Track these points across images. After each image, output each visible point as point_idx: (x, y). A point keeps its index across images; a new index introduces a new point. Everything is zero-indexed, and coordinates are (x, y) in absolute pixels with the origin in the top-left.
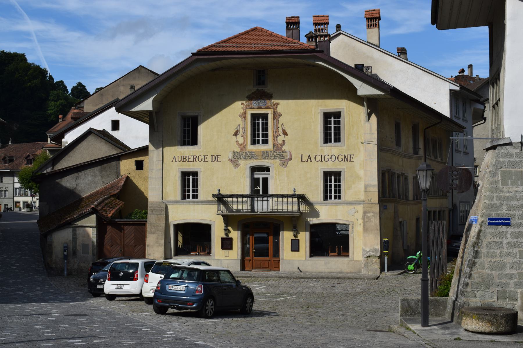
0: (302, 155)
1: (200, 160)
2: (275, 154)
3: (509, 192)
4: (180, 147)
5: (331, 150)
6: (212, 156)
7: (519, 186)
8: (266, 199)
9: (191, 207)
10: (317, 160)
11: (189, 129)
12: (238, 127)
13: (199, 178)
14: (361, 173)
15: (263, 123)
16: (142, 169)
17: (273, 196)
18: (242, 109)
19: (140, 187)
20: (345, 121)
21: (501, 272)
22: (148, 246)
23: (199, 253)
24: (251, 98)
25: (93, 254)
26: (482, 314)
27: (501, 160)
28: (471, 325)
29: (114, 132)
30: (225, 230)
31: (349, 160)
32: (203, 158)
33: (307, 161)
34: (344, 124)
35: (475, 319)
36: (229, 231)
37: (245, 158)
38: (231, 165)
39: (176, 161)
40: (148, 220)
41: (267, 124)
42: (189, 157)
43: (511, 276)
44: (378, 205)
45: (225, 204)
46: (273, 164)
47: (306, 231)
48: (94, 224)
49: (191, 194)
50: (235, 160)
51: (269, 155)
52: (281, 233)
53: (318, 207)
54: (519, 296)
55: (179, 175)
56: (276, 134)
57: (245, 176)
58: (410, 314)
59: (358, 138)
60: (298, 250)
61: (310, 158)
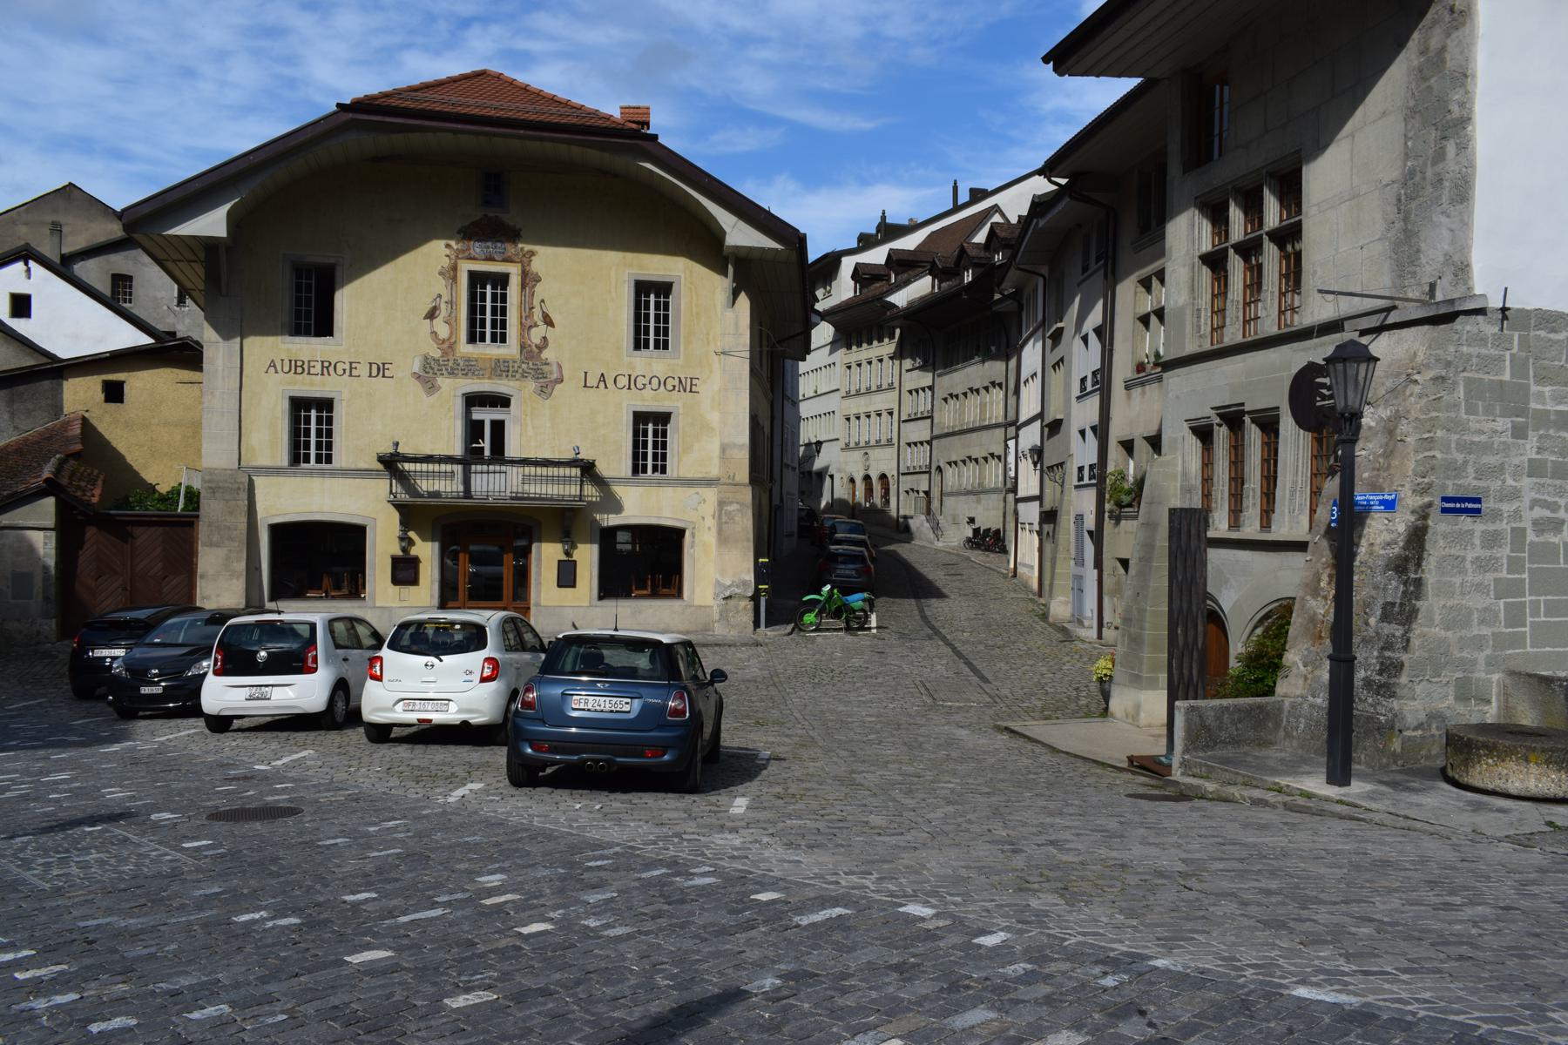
0: (586, 373)
1: (340, 371)
2: (524, 366)
3: (1481, 432)
4: (288, 339)
5: (650, 364)
6: (370, 364)
7: (1498, 419)
8: (497, 468)
9: (316, 483)
10: (620, 385)
11: (311, 297)
12: (435, 299)
13: (335, 414)
14: (714, 418)
15: (494, 296)
16: (121, 401)
17: (513, 462)
18: (447, 259)
19: (114, 443)
20: (681, 303)
21: (1463, 633)
22: (202, 577)
23: (326, 592)
24: (469, 233)
25: (46, 599)
26: (1558, 749)
27: (1465, 349)
28: (1522, 781)
29: (16, 320)
30: (401, 539)
31: (688, 389)
32: (347, 367)
33: (597, 387)
34: (678, 310)
35: (1536, 763)
36: (411, 542)
37: (452, 373)
38: (417, 388)
39: (276, 372)
40: (202, 513)
41: (504, 298)
42: (312, 364)
43: (1479, 643)
44: (750, 488)
45: (403, 478)
46: (520, 390)
47: (591, 543)
48: (51, 522)
49: (313, 452)
50: (428, 375)
51: (511, 369)
52: (534, 546)
53: (619, 490)
54: (1494, 690)
55: (286, 404)
56: (528, 323)
57: (452, 414)
58: (1205, 746)
59: (708, 343)
60: (574, 586)
61: (604, 381)
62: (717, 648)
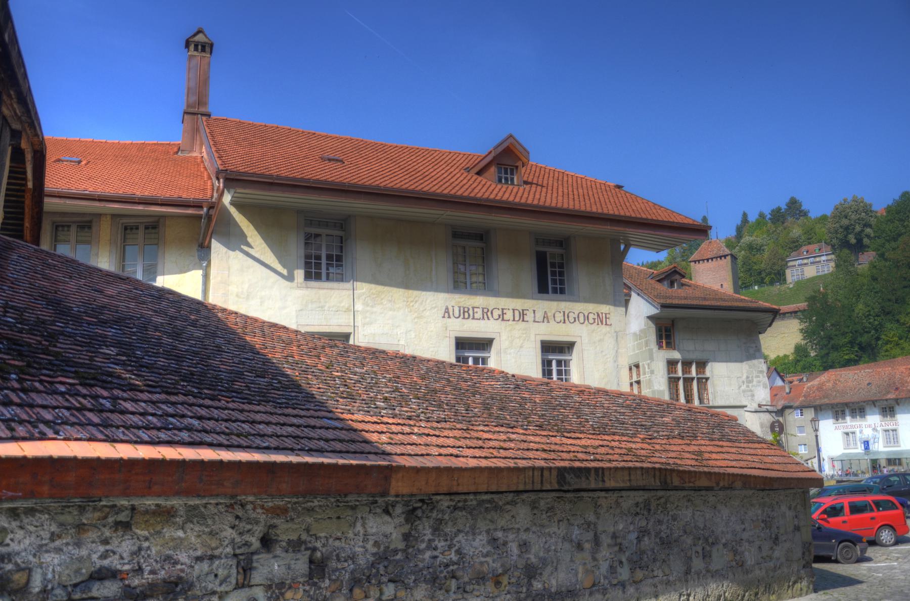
10: (558, 319)
31: (604, 323)
32: (500, 312)
39: (449, 317)
42: (476, 310)
62: (413, 453)
